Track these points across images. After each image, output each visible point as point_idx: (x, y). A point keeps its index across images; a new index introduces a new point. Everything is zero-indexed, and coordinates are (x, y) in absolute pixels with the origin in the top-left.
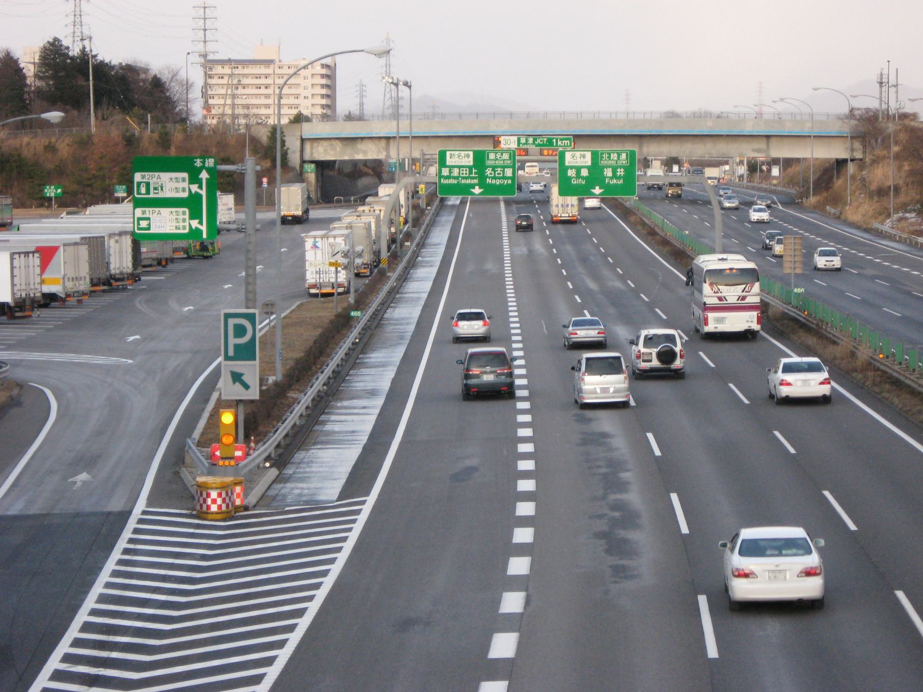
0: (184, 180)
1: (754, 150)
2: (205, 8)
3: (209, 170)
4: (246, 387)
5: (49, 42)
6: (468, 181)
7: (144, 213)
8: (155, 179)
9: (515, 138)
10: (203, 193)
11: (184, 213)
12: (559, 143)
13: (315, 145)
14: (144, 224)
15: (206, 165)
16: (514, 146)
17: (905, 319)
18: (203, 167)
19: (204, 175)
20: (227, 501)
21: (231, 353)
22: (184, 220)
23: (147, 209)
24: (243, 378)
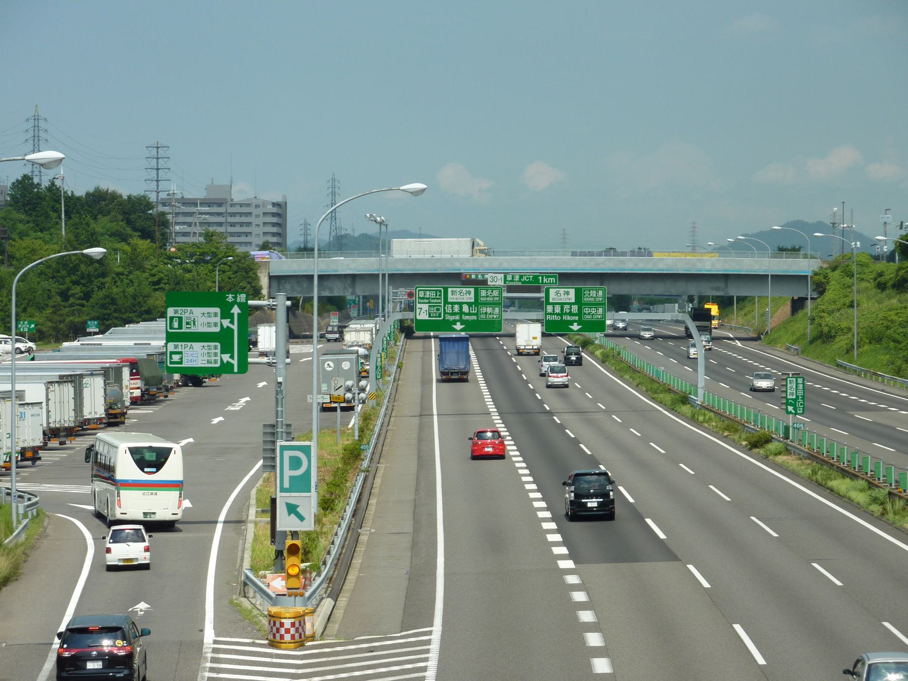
0: (216, 315)
1: (712, 289)
2: (158, 148)
3: (240, 305)
4: (302, 518)
5: (17, 180)
6: (569, 318)
7: (176, 347)
8: (187, 314)
9: (502, 276)
10: (235, 327)
11: (216, 348)
12: (545, 280)
13: (282, 281)
14: (176, 358)
15: (238, 301)
16: (500, 283)
17: (95, 434)
18: (235, 303)
19: (236, 310)
20: (300, 630)
21: (286, 485)
22: (216, 355)
23: (180, 344)
24: (298, 509)
